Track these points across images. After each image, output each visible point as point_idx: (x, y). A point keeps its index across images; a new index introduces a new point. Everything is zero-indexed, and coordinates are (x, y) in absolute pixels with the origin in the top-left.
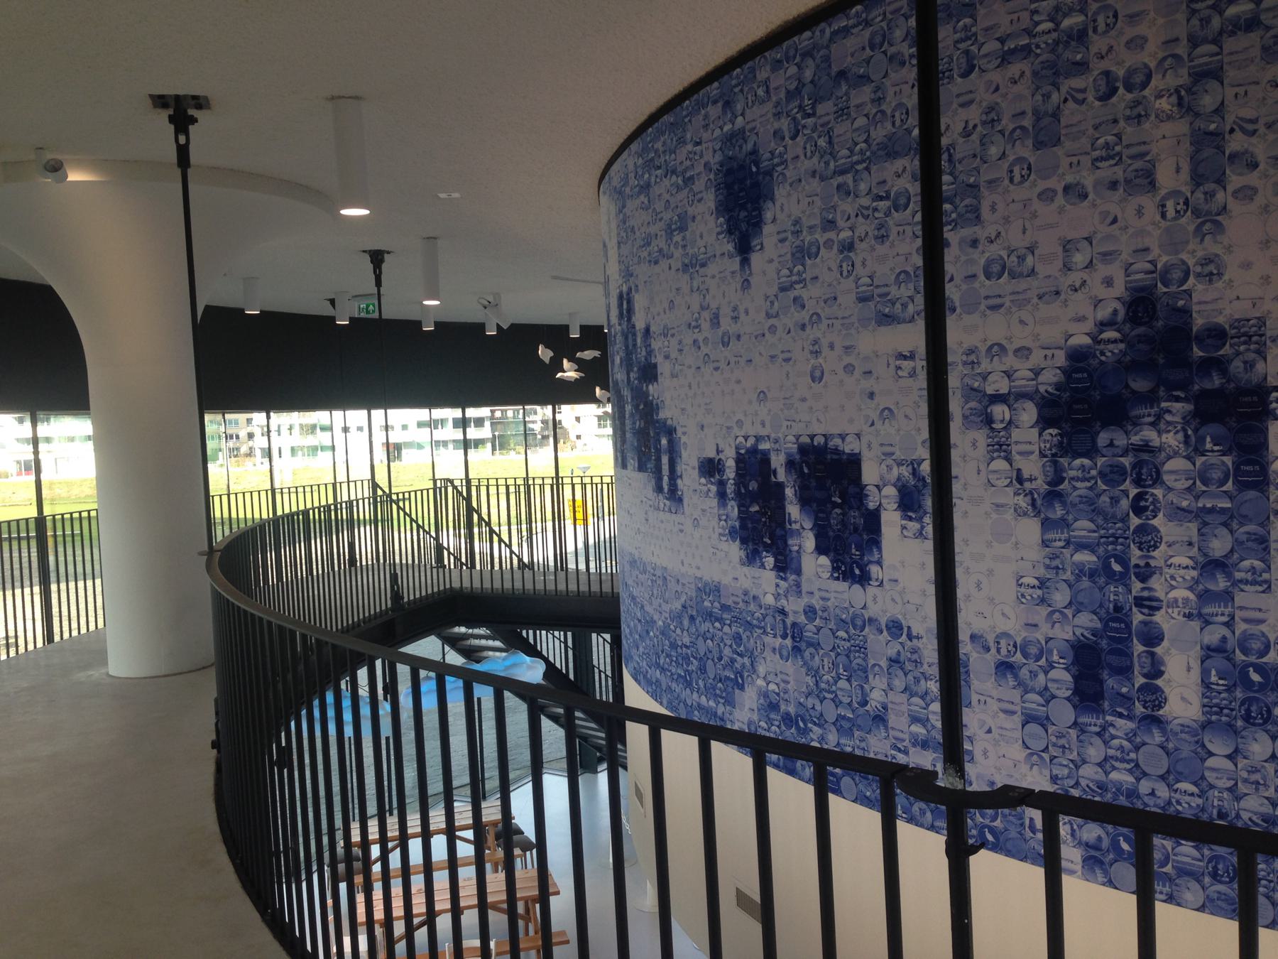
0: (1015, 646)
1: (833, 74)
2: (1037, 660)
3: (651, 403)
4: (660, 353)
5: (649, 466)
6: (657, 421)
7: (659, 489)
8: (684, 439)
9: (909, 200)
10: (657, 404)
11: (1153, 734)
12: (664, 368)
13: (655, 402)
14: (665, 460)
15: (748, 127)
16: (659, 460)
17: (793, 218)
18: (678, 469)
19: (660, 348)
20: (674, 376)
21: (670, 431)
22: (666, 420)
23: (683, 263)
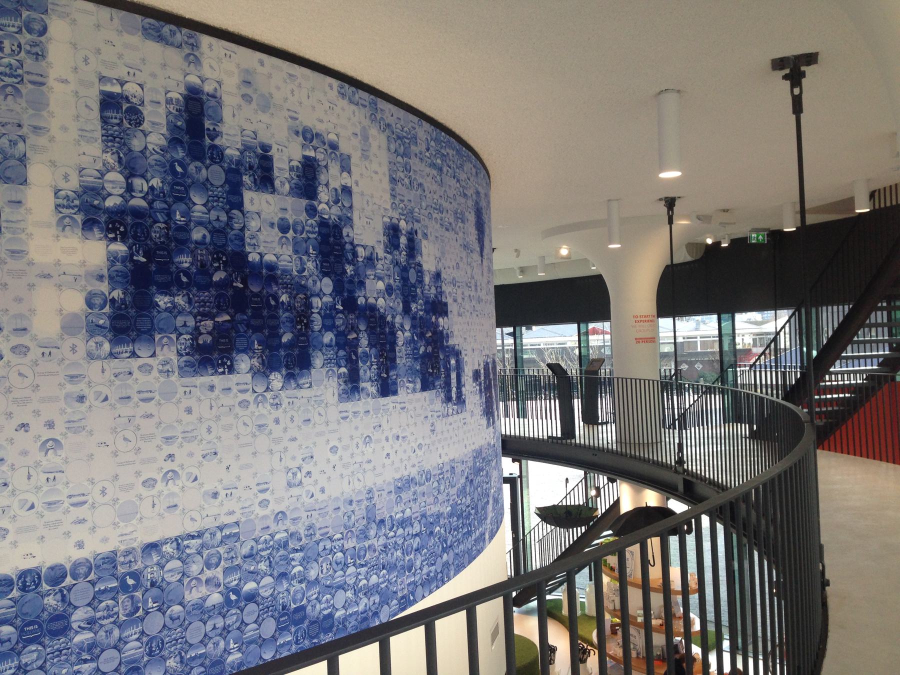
0: (19, 46)
1: (377, 521)
2: (301, 235)
3: (442, 332)
4: (451, 296)
5: (437, 383)
6: (448, 347)
7: (448, 399)
8: (466, 359)
9: (220, 559)
10: (447, 334)
11: (177, 151)
12: (452, 307)
13: (445, 332)
14: (453, 375)
15: (413, 516)
16: (448, 376)
17: (367, 488)
18: (463, 380)
19: (450, 293)
20: (460, 315)
21: (457, 354)
22: (454, 345)
23: (451, 466)
